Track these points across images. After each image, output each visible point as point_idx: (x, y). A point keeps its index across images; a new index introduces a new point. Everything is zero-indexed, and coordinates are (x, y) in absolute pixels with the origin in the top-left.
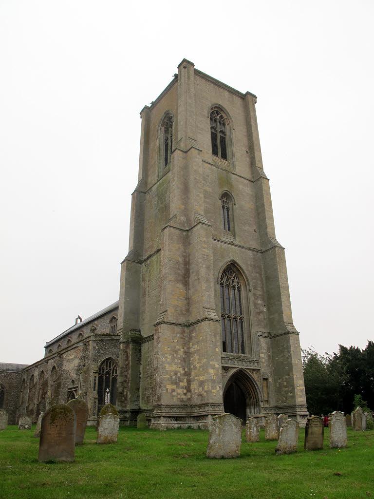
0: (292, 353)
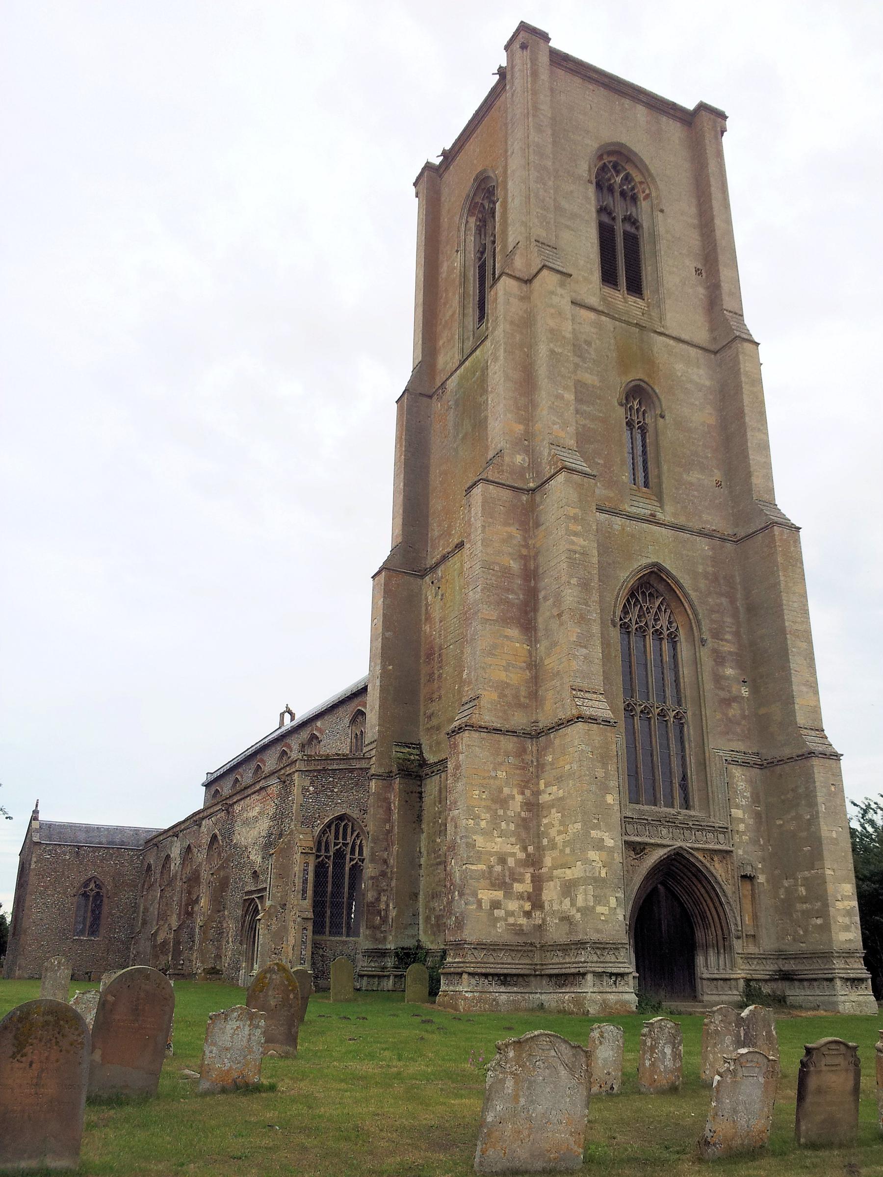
0: (822, 808)
